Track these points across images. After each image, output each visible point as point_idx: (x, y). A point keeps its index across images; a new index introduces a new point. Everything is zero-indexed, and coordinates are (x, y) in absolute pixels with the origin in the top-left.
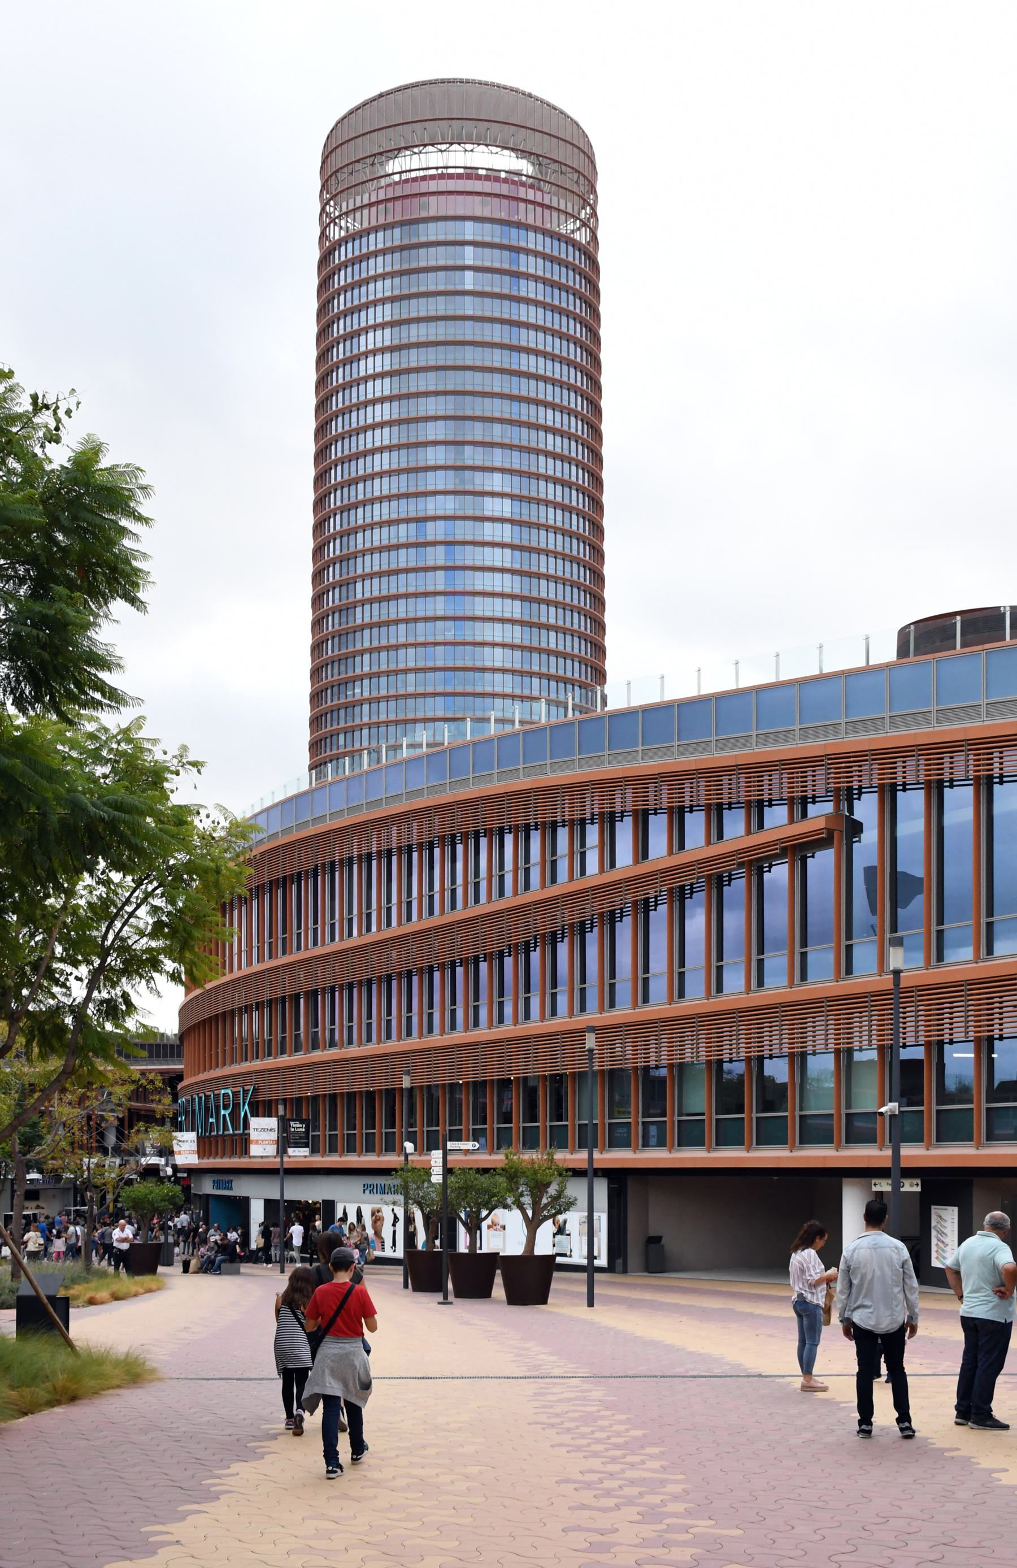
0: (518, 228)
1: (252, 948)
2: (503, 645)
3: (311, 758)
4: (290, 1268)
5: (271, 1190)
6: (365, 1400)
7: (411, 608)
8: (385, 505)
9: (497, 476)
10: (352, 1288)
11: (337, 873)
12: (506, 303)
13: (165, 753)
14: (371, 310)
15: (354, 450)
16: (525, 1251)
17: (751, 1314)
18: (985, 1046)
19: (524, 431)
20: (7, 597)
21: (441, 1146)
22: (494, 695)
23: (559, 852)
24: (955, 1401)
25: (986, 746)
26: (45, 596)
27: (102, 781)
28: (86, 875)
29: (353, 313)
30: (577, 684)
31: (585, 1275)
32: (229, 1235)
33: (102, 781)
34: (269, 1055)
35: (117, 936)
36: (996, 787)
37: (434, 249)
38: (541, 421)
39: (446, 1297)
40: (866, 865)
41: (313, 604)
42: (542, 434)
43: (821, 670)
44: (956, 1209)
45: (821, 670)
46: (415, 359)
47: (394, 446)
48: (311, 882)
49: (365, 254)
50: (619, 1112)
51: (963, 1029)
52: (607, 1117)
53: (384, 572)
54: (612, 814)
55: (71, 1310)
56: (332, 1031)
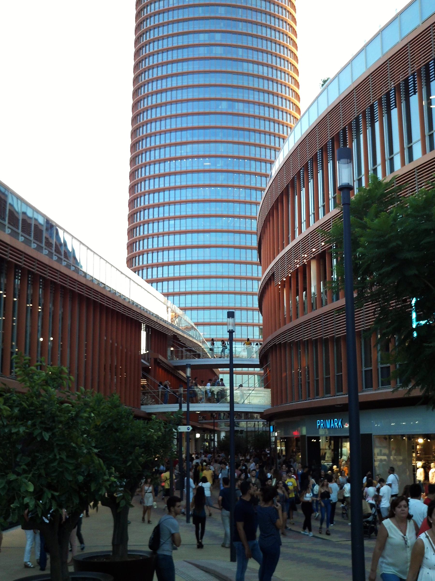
1: (318, 208)
5: (364, 367)
7: (248, 225)
8: (166, 223)
10: (239, 138)
11: (362, 136)
12: (250, 51)
15: (149, 132)
17: (361, 344)
18: (427, 468)
19: (251, 65)
21: (40, 344)
22: (250, 173)
27: (248, 457)
31: (228, 370)
33: (248, 457)
40: (229, 559)
44: (259, 363)
46: (187, 67)
47: (173, 116)
49: (151, 79)
52: (324, 375)
56: (375, 170)
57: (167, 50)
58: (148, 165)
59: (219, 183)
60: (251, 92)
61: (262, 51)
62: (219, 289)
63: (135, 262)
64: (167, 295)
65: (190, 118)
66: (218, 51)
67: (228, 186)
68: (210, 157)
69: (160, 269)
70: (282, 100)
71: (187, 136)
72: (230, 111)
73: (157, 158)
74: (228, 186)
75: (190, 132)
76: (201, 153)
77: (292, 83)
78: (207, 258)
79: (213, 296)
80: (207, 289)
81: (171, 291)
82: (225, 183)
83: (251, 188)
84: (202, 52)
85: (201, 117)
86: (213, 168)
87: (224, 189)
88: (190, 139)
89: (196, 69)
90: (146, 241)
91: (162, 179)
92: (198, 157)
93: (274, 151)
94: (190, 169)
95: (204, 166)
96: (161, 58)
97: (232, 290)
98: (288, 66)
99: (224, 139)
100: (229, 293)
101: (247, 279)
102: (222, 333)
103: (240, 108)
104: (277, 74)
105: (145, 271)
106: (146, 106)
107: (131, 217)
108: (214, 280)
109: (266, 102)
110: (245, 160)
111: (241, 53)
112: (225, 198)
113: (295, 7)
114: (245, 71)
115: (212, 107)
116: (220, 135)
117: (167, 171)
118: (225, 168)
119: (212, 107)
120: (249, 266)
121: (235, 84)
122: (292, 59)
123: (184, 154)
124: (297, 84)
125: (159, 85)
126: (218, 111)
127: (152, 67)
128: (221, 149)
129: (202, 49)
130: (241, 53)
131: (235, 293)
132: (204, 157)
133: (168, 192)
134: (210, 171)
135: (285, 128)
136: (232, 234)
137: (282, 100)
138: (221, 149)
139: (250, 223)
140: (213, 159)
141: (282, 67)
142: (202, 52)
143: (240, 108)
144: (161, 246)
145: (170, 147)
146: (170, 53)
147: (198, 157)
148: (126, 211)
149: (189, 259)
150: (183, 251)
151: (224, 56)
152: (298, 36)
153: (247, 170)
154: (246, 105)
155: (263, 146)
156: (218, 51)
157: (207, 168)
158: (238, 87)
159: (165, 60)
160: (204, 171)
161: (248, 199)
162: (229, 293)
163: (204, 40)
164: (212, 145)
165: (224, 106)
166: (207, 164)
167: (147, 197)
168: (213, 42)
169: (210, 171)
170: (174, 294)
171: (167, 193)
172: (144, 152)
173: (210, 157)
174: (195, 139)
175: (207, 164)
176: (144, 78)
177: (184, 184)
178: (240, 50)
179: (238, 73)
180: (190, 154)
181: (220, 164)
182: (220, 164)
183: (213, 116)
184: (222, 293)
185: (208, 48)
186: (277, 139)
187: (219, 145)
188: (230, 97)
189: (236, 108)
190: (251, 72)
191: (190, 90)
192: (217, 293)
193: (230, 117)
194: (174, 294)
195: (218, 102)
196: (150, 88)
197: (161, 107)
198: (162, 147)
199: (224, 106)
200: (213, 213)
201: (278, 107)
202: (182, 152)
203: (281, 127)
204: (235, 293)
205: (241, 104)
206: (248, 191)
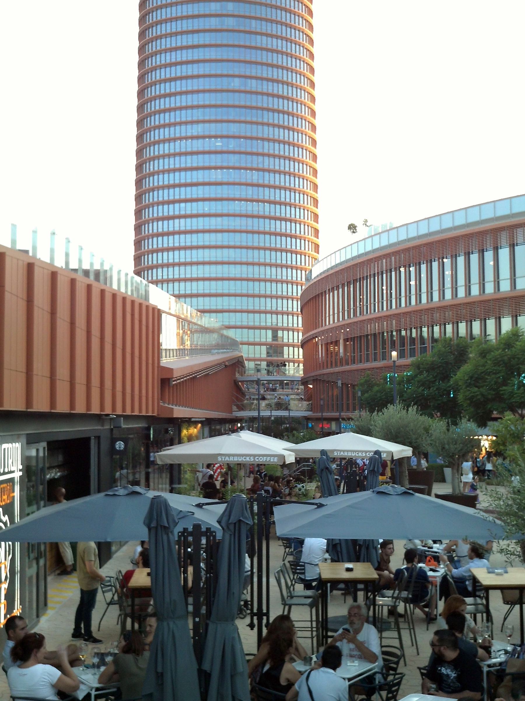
0: (262, 50)
2: (246, 138)
3: (136, 220)
4: (433, 628)
6: (361, 540)
9: (237, 80)
13: (352, 228)
14: (157, 116)
15: (159, 33)
16: (358, 640)
20: (521, 383)
23: (472, 282)
24: (42, 259)
25: (512, 228)
26: (282, 468)
28: (319, 494)
29: (156, 55)
30: (289, 55)
32: (123, 447)
34: (361, 362)
35: (271, 485)
36: (471, 255)
37: (220, 124)
38: (276, 107)
39: (405, 620)
41: (139, 51)
42: (277, 145)
43: (210, 220)
45: (210, 220)
46: (197, 40)
48: (372, 279)
50: (106, 283)
51: (290, 294)
53: (178, 32)
54: (514, 244)
55: (175, 416)
57: (174, 170)
58: (156, 189)
59: (231, 164)
60: (265, 68)
61: (278, 97)
62: (232, 228)
63: (145, 214)
64: (178, 296)
65: (201, 80)
66: (230, 23)
67: (240, 168)
68: (222, 137)
69: (171, 238)
70: (295, 17)
71: (198, 114)
72: (242, 88)
73: (168, 46)
74: (240, 168)
75: (201, 110)
76: (213, 133)
77: (306, 42)
78: (219, 212)
79: (226, 234)
80: (219, 259)
81: (182, 292)
82: (237, 165)
83: (264, 170)
84: (214, 23)
85: (213, 34)
86: (225, 149)
87: (237, 171)
88: (201, 118)
89: (207, 42)
90: (156, 162)
91: (173, 83)
92: (210, 137)
93: (289, 207)
94: (201, 149)
95: (216, 146)
96: (168, 58)
97: (244, 228)
98: (303, 23)
99: (237, 118)
100: (241, 232)
101: (258, 201)
102: (234, 320)
103: (253, 85)
104: (291, 32)
105: (155, 208)
106: (154, 79)
107: (140, 108)
108: (227, 266)
109: (279, 34)
110: (257, 140)
111: (254, 25)
112: (237, 180)
113: (313, 40)
114: (259, 45)
115: (224, 83)
116: (233, 114)
117: (179, 75)
118: (237, 149)
119: (224, 83)
120: (261, 220)
121: (248, 59)
122: (307, 30)
123: (195, 134)
124: (311, 27)
125: (168, 58)
126: (231, 88)
127: (160, 37)
128: (234, 129)
129: (213, 20)
130: (254, 25)
131: (247, 232)
132: (216, 137)
133: (179, 127)
134: (221, 152)
135: (297, 32)
136: (245, 218)
137: (295, 17)
138: (234, 129)
139: (262, 144)
140: (225, 140)
141: (296, 10)
142: (214, 23)
143: (253, 85)
144: (172, 167)
145: (181, 110)
146: (179, 37)
147: (210, 137)
148: (133, 146)
149: (201, 164)
150: (195, 157)
151: (236, 28)
152: (314, 30)
153: (260, 120)
154: (259, 82)
155: (277, 140)
156: (230, 23)
157: (219, 149)
158: (250, 62)
159: (174, 45)
160: (216, 152)
161: (261, 182)
162: (241, 232)
163: (216, 10)
164: (224, 125)
165: (236, 84)
166: (219, 144)
167: (158, 86)
168: (224, 12)
169: (221, 152)
170: (185, 296)
171: (178, 128)
172: (154, 25)
173: (222, 137)
174: (207, 118)
175: (219, 144)
176: (150, 48)
177: (195, 103)
178: (253, 22)
179: (251, 108)
180: (201, 134)
181: (232, 145)
182: (232, 145)
183: (224, 64)
184: (234, 231)
185: (220, 18)
186: (289, 29)
187: (231, 125)
188: (242, 73)
189: (249, 85)
190: (264, 46)
191: (201, 65)
192: (228, 231)
193: (242, 65)
194: (185, 296)
195: (230, 79)
196: (158, 75)
197: (171, 6)
198: (173, 20)
199: (236, 84)
200: (225, 196)
201: (291, 10)
202: (193, 131)
203: (293, 16)
204: (247, 232)
205: (254, 81)
206: (261, 173)
